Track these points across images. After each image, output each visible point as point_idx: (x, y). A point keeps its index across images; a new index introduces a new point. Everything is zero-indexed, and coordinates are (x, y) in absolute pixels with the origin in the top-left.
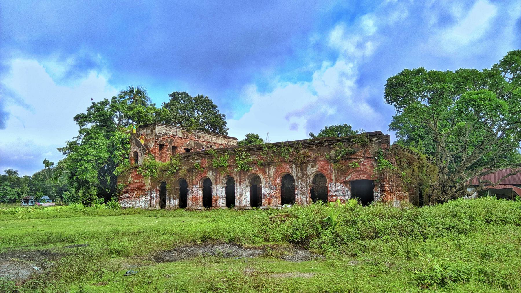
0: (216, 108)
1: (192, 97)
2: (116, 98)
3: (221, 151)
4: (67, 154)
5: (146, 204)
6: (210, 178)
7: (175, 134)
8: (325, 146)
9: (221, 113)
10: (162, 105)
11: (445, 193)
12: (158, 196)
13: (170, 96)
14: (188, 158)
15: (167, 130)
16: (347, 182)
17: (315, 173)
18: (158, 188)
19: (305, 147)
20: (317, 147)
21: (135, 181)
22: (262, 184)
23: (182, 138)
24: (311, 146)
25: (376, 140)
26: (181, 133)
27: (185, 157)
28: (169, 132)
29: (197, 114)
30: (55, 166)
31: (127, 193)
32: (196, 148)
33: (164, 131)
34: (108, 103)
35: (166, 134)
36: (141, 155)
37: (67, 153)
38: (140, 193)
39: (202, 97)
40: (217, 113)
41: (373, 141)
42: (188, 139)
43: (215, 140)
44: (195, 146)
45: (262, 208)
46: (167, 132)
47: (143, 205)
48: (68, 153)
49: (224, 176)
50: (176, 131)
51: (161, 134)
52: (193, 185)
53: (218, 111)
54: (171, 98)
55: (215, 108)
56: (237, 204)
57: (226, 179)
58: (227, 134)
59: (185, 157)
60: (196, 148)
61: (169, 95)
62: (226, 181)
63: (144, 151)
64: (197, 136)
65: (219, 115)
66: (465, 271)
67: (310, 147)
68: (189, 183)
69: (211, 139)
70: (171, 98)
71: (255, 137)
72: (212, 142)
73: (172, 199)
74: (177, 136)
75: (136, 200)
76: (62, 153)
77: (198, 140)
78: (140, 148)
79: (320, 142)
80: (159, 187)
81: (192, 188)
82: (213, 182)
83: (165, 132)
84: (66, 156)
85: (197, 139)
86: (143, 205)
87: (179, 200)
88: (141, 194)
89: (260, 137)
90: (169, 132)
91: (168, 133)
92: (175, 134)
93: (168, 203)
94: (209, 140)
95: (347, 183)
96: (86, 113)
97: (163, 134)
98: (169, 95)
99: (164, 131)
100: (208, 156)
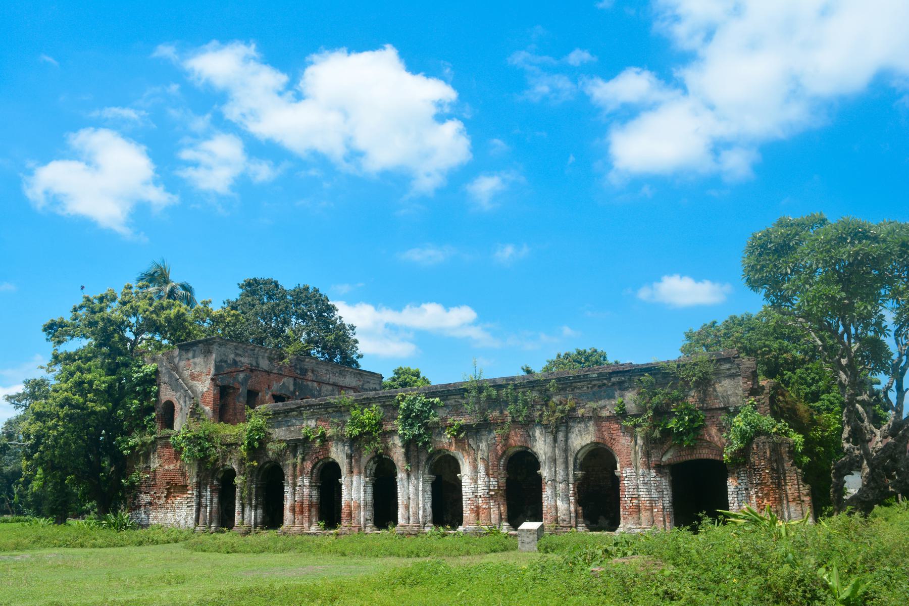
0: (336, 312)
1: (285, 288)
2: (131, 288)
3: (364, 399)
4: (24, 408)
5: (189, 518)
6: (337, 461)
7: (254, 364)
8: (610, 384)
9: (347, 321)
10: (223, 305)
11: (877, 483)
12: (215, 500)
13: (241, 288)
14: (286, 416)
15: (237, 355)
16: (664, 467)
17: (587, 448)
18: (215, 482)
19: (564, 389)
20: (592, 388)
21: (166, 467)
22: (462, 474)
23: (268, 372)
24: (579, 384)
25: (729, 369)
26: (267, 362)
27: (279, 414)
28: (242, 359)
29: (296, 323)
30: (896, 361)
31: (148, 493)
32: (297, 393)
33: (232, 356)
34: (115, 299)
35: (235, 363)
36: (181, 409)
37: (23, 406)
38: (176, 495)
39: (306, 289)
40: (338, 322)
41: (721, 372)
42: (281, 374)
43: (337, 378)
44: (295, 389)
45: (465, 530)
46: (238, 359)
47: (182, 522)
48: (25, 406)
49: (370, 456)
50: (257, 358)
51: (226, 362)
52: (295, 477)
53: (340, 318)
54: (241, 291)
55: (332, 311)
56: (401, 520)
57: (375, 463)
58: (358, 365)
59: (279, 414)
60: (297, 393)
61: (239, 284)
62: (374, 469)
63: (187, 399)
64: (301, 369)
65: (343, 325)
66: (188, 500)
67: (575, 387)
68: (288, 472)
69: (328, 376)
70: (241, 291)
71: (413, 375)
72: (331, 381)
73: (247, 509)
74: (258, 367)
75: (167, 508)
76: (14, 405)
77: (301, 377)
78: (179, 394)
79: (598, 377)
80: (218, 480)
81: (294, 485)
82: (344, 469)
83: (234, 359)
84: (20, 412)
85: (300, 374)
86: (182, 522)
87: (264, 512)
88: (178, 496)
89: (422, 375)
90: (242, 359)
91: (240, 361)
92: (254, 364)
93: (237, 519)
94: (325, 378)
95: (664, 468)
96: (68, 318)
97: (229, 362)
98: (239, 284)
99: (232, 356)
100: (334, 411)
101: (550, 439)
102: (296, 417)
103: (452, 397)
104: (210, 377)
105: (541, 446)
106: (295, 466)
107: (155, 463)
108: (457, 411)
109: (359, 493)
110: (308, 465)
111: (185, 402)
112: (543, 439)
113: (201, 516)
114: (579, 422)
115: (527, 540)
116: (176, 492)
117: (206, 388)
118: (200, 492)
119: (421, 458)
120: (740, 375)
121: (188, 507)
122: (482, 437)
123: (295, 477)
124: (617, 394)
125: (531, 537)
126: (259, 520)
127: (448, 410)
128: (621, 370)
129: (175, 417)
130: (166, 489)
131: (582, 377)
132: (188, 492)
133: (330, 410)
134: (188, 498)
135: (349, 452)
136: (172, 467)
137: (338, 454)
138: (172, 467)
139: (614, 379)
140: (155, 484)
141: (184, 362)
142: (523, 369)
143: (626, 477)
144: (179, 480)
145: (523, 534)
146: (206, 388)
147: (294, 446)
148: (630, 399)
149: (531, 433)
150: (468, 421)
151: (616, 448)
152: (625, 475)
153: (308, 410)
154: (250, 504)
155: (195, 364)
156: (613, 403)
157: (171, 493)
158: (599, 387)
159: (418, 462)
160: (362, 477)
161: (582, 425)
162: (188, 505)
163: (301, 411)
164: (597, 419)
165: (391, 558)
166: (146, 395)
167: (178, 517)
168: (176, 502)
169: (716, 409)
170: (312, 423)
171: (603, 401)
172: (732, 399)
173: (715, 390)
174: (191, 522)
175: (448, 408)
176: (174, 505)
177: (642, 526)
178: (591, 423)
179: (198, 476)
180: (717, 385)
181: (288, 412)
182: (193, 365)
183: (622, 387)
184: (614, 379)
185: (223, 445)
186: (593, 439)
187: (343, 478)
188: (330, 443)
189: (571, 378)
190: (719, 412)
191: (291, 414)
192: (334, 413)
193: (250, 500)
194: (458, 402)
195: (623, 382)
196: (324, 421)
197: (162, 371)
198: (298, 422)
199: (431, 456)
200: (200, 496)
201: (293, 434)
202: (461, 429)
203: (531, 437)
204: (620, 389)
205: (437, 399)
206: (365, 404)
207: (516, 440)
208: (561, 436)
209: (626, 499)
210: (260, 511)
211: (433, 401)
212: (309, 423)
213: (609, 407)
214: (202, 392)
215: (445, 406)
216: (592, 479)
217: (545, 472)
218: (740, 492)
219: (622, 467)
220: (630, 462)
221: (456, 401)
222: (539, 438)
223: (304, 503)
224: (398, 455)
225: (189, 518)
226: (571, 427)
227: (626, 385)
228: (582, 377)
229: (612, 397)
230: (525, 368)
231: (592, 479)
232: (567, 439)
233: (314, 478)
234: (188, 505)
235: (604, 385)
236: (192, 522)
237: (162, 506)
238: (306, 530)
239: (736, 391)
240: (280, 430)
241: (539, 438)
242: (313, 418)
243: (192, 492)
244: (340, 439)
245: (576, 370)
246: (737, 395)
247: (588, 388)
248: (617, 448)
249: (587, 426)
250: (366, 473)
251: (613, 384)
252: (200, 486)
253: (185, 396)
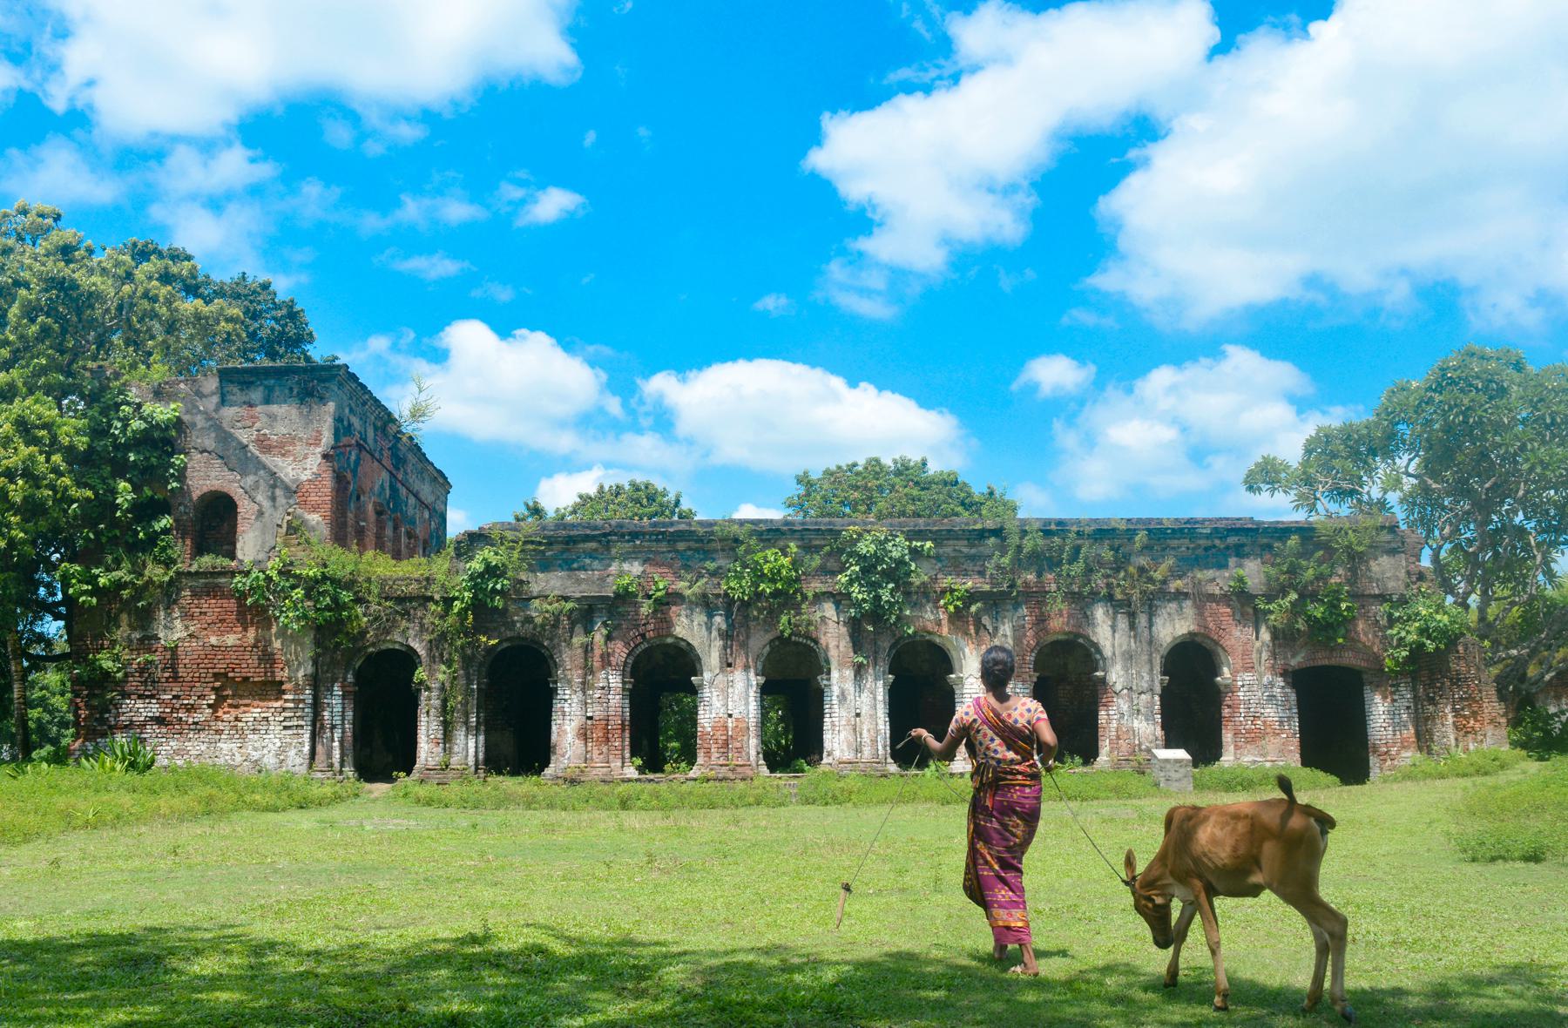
5: (292, 753)
8: (1222, 546)
12: (350, 714)
21: (213, 640)
25: (1389, 542)
31: (152, 697)
36: (261, 513)
52: (588, 670)
63: (278, 492)
75: (219, 732)
100: (689, 549)
101: (1123, 623)
102: (592, 555)
103: (951, 542)
104: (319, 450)
105: (1106, 632)
106: (587, 649)
107: (173, 630)
108: (957, 566)
109: (747, 704)
110: (620, 651)
111: (273, 499)
112: (1110, 623)
113: (319, 748)
114: (1169, 601)
115: (1174, 776)
116: (241, 697)
117: (308, 472)
118: (316, 698)
119: (879, 643)
120: (1403, 552)
121: (285, 728)
122: (1006, 614)
123: (588, 670)
124: (1232, 561)
125: (1182, 770)
126: (481, 756)
127: (939, 565)
128: (1238, 526)
129: (240, 528)
130: (213, 689)
131: (1186, 531)
132: (286, 697)
133: (681, 546)
134: (284, 709)
135: (724, 627)
136: (231, 639)
137: (689, 628)
138: (231, 639)
139: (1232, 540)
140: (176, 678)
141: (234, 409)
142: (527, 505)
143: (1243, 686)
144: (251, 668)
145: (1168, 766)
146: (308, 472)
147: (586, 613)
148: (1253, 573)
149: (1089, 613)
150: (978, 585)
151: (1227, 642)
152: (1240, 683)
153: (628, 541)
154: (466, 723)
155: (272, 417)
156: (1227, 575)
157: (225, 698)
158: (1206, 549)
159: (876, 652)
160: (752, 674)
161: (1173, 606)
162: (285, 724)
163: (608, 541)
164: (1202, 600)
165: (904, 812)
166: (146, 475)
167: (255, 749)
168: (248, 717)
169: (1370, 596)
170: (636, 568)
171: (1211, 571)
172: (1391, 584)
173: (1369, 569)
174: (296, 759)
175: (941, 561)
176: (240, 724)
177: (1269, 758)
178: (1189, 603)
179: (315, 662)
180: (1372, 563)
181: (575, 542)
182: (264, 419)
183: (1240, 552)
184: (1232, 540)
185: (387, 599)
186: (1193, 628)
187: (707, 675)
188: (674, 608)
189: (1169, 531)
190: (1371, 600)
191: (581, 545)
192: (689, 553)
193: (467, 715)
194: (960, 551)
195: (1243, 545)
196: (663, 565)
197: (194, 425)
198: (596, 562)
199: (781, 642)
200: (317, 707)
201: (583, 587)
202: (971, 597)
203: (1088, 619)
204: (1238, 555)
205: (929, 544)
206: (769, 540)
207: (1059, 622)
208: (1142, 620)
209: (1242, 719)
210: (482, 738)
211: (922, 546)
212: (626, 566)
213: (1218, 580)
214: (297, 480)
215: (938, 558)
216: (1088, 692)
217: (1116, 676)
218: (1397, 712)
219: (1234, 673)
220: (1251, 665)
221: (955, 550)
222: (1104, 622)
223: (612, 722)
224: (834, 638)
225: (292, 753)
226: (1157, 607)
227: (1247, 549)
228: (1186, 531)
229: (1223, 566)
230: (531, 504)
231: (1088, 692)
232: (1151, 625)
233: (628, 675)
234: (285, 724)
235: (1214, 546)
236: (298, 760)
237: (198, 727)
238: (616, 774)
239: (1397, 573)
240: (551, 575)
241: (1104, 622)
242: (636, 558)
243: (298, 692)
244: (706, 604)
245: (618, 515)
246: (1398, 579)
247: (1188, 548)
248: (1228, 643)
249: (1181, 608)
250: (756, 669)
251: (1228, 548)
252: (318, 683)
253: (274, 487)
